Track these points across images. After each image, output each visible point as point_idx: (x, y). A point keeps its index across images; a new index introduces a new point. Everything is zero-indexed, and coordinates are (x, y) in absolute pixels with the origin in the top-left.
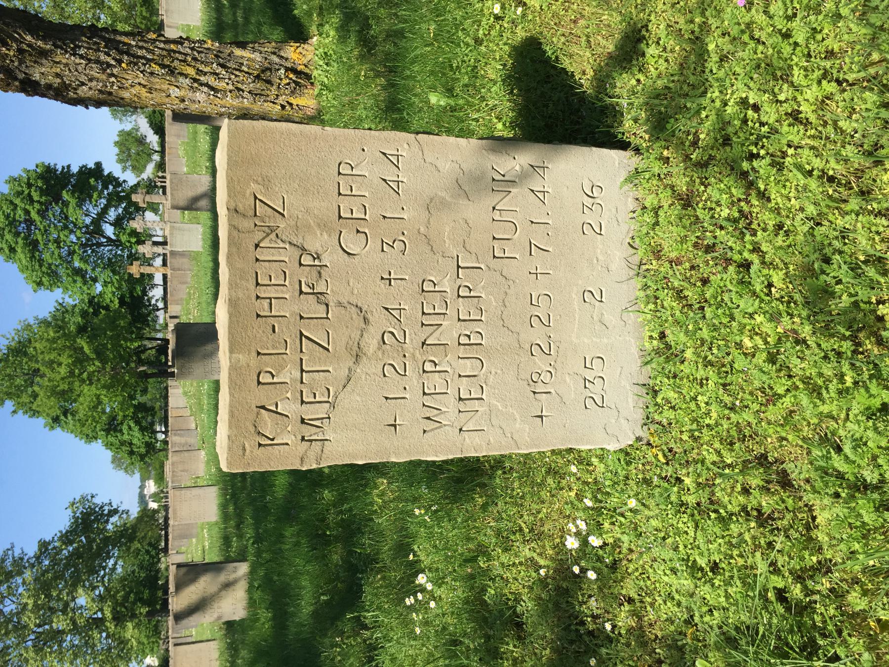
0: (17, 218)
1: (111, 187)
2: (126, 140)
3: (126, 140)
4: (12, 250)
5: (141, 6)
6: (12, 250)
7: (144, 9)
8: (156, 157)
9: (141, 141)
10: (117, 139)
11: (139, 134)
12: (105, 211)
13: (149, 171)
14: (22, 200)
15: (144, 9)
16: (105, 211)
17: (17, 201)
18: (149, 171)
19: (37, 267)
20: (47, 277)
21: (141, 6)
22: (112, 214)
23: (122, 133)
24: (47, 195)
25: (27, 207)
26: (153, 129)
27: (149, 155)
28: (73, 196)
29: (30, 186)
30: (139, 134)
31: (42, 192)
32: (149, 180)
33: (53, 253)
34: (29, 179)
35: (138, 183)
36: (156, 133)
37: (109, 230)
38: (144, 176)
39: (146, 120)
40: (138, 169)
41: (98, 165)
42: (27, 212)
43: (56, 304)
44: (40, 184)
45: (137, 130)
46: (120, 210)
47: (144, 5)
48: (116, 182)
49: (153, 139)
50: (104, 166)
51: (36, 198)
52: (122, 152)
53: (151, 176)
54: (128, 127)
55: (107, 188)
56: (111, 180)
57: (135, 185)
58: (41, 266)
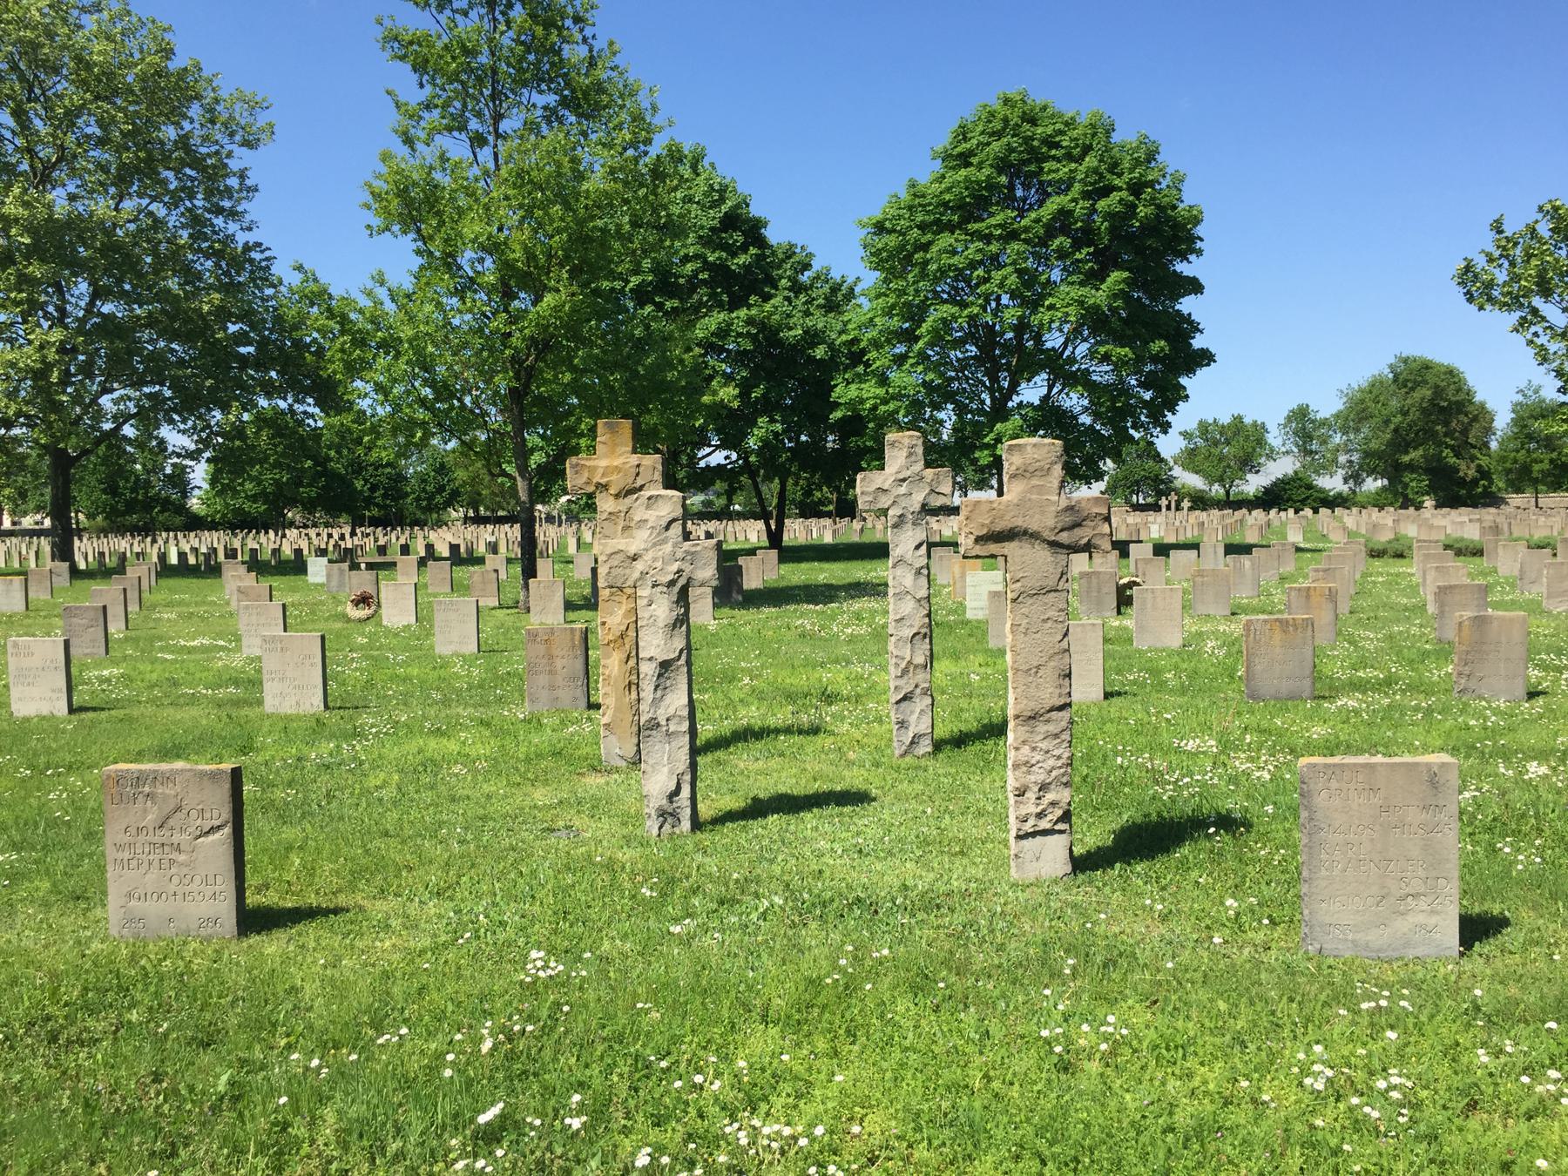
0: (1047, 166)
1: (1147, 396)
2: (1247, 437)
3: (1247, 437)
4: (964, 159)
5: (1551, 461)
6: (964, 159)
7: (1546, 466)
8: (1217, 490)
9: (1248, 463)
10: (1248, 420)
11: (1262, 460)
12: (1079, 379)
13: (1189, 480)
14: (1096, 171)
15: (1546, 466)
16: (1079, 379)
17: (1090, 161)
18: (1189, 480)
19: (919, 218)
20: (896, 253)
21: (1551, 461)
22: (1074, 401)
23: (1259, 431)
24: (1112, 230)
25: (1077, 187)
26: (1275, 484)
27: (1221, 480)
28: (1115, 296)
29: (1136, 188)
30: (1262, 460)
31: (1119, 220)
32: (1171, 479)
33: (954, 253)
34: (1151, 184)
35: (1162, 460)
36: (1267, 491)
37: (1032, 392)
38: (1177, 471)
39: (1291, 473)
40: (1190, 459)
41: (1206, 357)
42: (1064, 186)
43: (850, 280)
44: (1142, 211)
45: (1269, 457)
46: (1086, 419)
47: (1556, 466)
48: (1158, 415)
49: (1253, 484)
50: (1203, 373)
51: (1102, 205)
52: (1222, 429)
53: (1177, 484)
54: (1275, 438)
55: (1145, 385)
56: (1171, 396)
57: (1158, 455)
58: (923, 227)
